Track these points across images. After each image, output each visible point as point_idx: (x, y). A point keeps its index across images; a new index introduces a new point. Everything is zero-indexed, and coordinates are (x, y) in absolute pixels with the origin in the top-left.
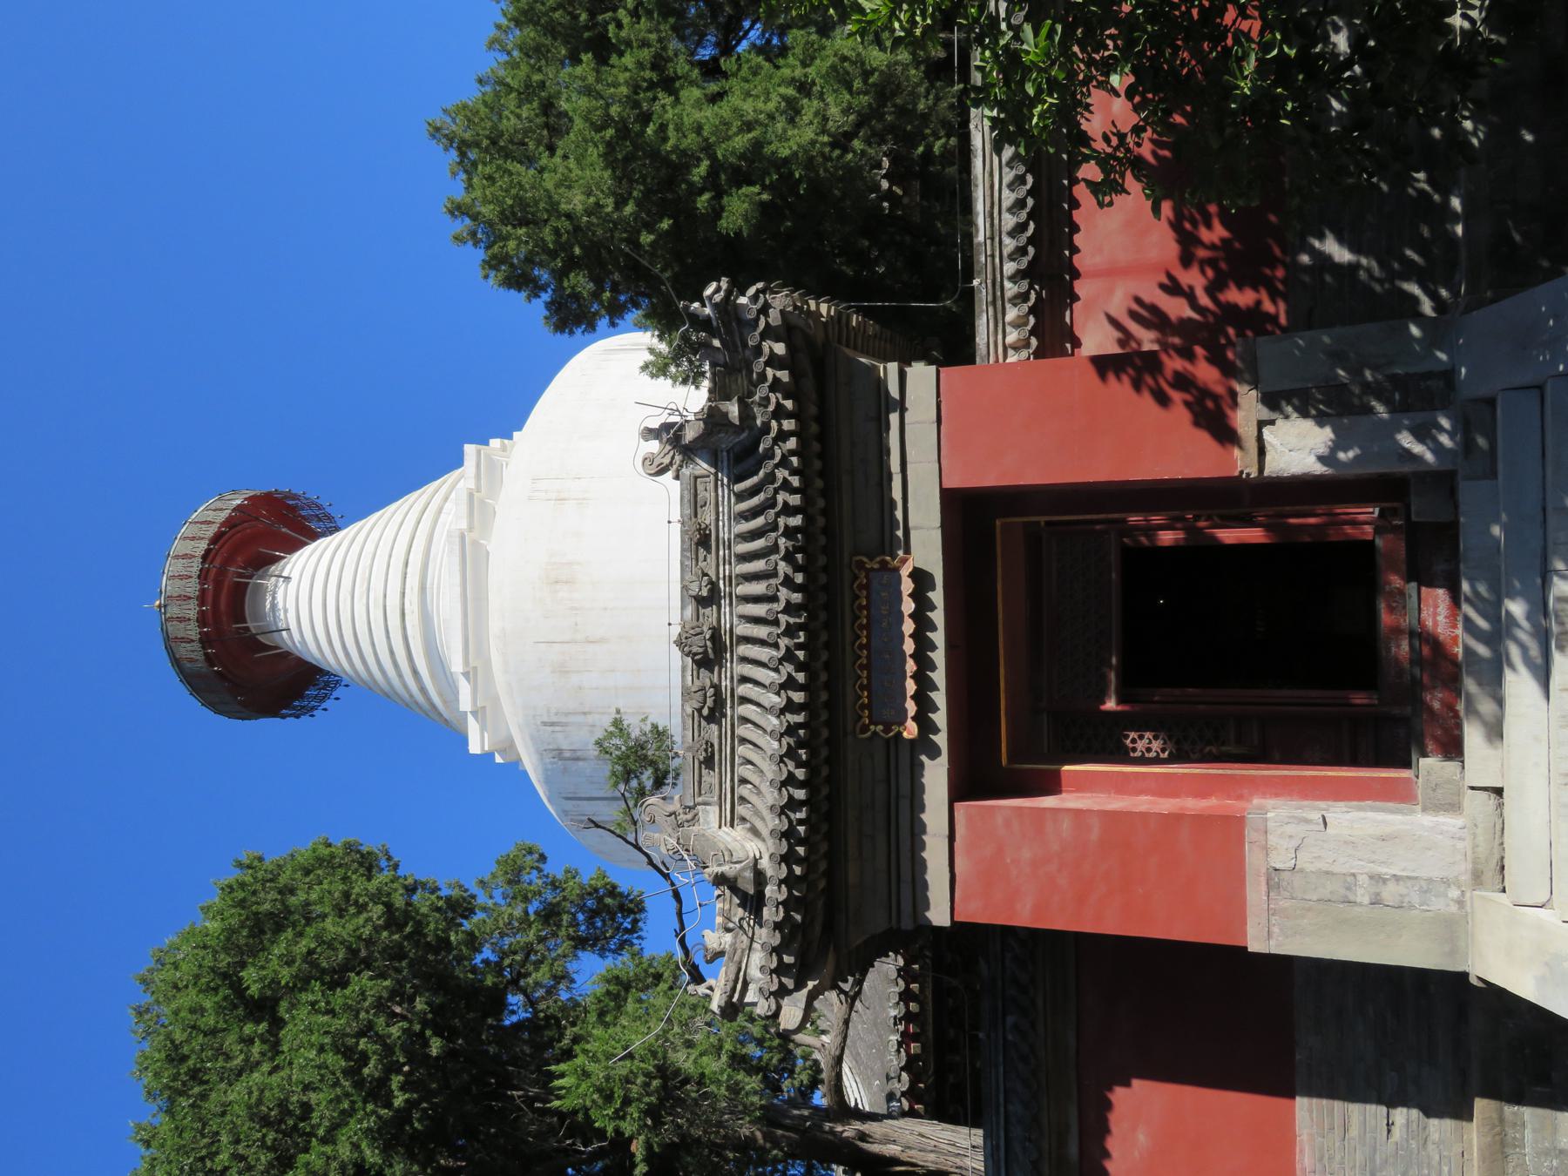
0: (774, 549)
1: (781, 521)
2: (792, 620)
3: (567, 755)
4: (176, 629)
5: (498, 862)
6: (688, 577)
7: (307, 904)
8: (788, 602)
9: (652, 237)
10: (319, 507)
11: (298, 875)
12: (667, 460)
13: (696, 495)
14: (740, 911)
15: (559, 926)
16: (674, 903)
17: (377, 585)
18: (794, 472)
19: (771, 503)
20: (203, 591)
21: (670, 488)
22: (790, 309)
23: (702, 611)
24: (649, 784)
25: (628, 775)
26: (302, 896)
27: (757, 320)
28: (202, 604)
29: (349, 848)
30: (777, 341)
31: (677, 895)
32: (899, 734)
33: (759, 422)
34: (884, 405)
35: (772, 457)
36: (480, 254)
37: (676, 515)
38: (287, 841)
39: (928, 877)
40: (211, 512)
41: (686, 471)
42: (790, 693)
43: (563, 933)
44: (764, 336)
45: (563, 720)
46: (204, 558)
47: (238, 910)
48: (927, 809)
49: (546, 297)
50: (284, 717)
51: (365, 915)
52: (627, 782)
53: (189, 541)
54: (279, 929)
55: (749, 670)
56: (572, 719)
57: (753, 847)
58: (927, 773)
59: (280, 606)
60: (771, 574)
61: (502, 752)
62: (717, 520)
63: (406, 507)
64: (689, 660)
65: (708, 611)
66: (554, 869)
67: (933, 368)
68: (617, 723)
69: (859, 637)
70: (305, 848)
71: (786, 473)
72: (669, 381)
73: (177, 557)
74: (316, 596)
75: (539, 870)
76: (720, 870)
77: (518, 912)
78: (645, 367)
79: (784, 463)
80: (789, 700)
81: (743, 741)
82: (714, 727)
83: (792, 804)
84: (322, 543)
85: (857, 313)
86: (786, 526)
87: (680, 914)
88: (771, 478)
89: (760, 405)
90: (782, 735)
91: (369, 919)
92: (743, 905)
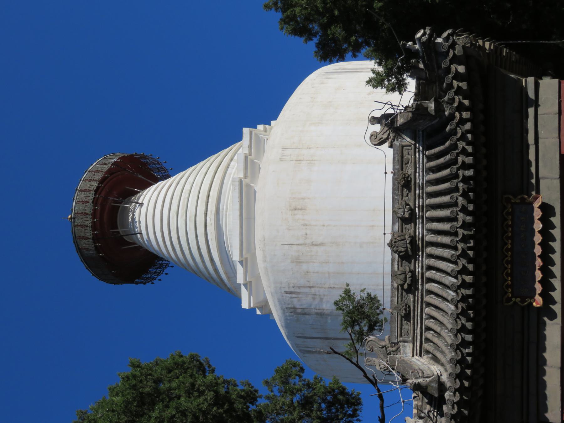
0: (456, 189)
1: (460, 173)
2: (466, 233)
3: (299, 311)
4: (80, 232)
5: (277, 371)
6: (397, 206)
7: (170, 389)
8: (464, 222)
9: (381, 4)
10: (159, 164)
11: (164, 372)
12: (385, 136)
13: (402, 157)
14: (428, 407)
15: (312, 411)
16: (379, 401)
17: (191, 208)
18: (468, 143)
19: (455, 161)
20: (95, 210)
21: (387, 153)
22: (468, 45)
23: (404, 226)
24: (366, 329)
25: (353, 323)
26: (167, 385)
27: (448, 51)
28: (94, 218)
29: (193, 358)
30: (460, 64)
31: (381, 397)
32: (531, 303)
33: (447, 113)
34: (526, 103)
35: (456, 133)
36: (279, 15)
37: (390, 168)
38: (157, 350)
39: (547, 392)
40: (99, 166)
41: (397, 143)
42: (464, 277)
43: (314, 414)
44: (452, 61)
45: (298, 290)
46: (96, 191)
47: (132, 391)
48: (547, 351)
49: (316, 40)
50: (137, 283)
51: (203, 398)
52: (353, 327)
53: (88, 180)
54: (153, 404)
55: (433, 262)
56: (302, 290)
57: (436, 369)
58: (547, 328)
59: (137, 219)
60: (455, 204)
61: (261, 308)
62: (415, 172)
63: (208, 164)
64: (396, 255)
65: (408, 226)
66: (309, 376)
67: (557, 81)
68: (347, 292)
69: (506, 244)
70: (167, 356)
71: (464, 144)
72: (384, 90)
73: (81, 191)
74: (162, 213)
75: (300, 377)
76: (417, 381)
77: (287, 401)
78: (369, 82)
79: (463, 138)
80: (463, 280)
81: (429, 305)
82: (411, 296)
83: (464, 344)
84: (161, 184)
85: (505, 47)
86: (464, 176)
87: (382, 407)
88: (454, 147)
89: (447, 103)
90: (458, 302)
91: (206, 400)
92: (429, 403)
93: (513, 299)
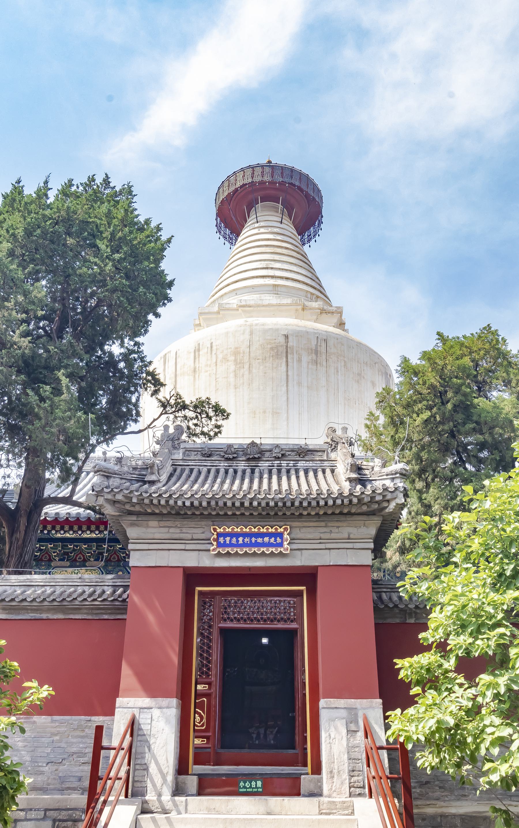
7: (125, 236)
28: (269, 182)
45: (214, 352)
93: (215, 533)
